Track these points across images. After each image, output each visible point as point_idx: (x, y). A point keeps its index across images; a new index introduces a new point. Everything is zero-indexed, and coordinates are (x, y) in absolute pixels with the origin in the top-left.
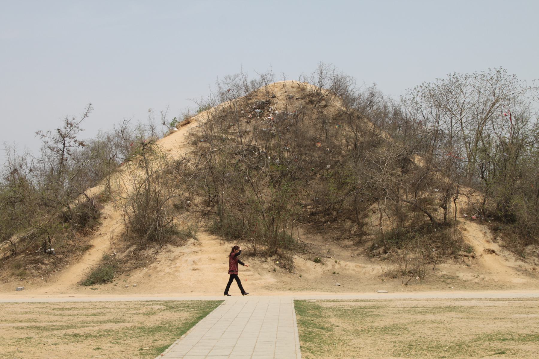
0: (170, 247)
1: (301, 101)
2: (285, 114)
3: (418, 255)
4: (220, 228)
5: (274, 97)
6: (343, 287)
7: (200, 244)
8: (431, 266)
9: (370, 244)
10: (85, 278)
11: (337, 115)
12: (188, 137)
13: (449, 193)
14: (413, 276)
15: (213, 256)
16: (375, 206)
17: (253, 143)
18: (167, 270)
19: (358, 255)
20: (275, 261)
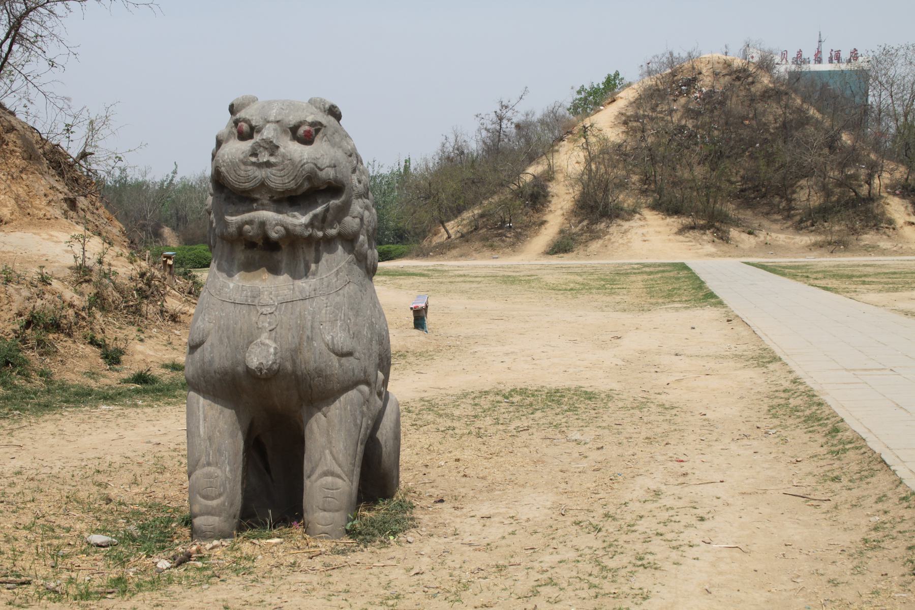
0: (620, 222)
1: (727, 78)
2: (712, 92)
3: (843, 227)
4: (660, 205)
5: (700, 73)
6: (775, 254)
7: (645, 219)
8: (855, 237)
9: (798, 218)
10: (548, 250)
11: (765, 92)
12: (617, 117)
13: (874, 169)
14: (838, 245)
15: (658, 229)
16: (803, 182)
17: (683, 122)
18: (621, 241)
19: (787, 228)
20: (713, 233)
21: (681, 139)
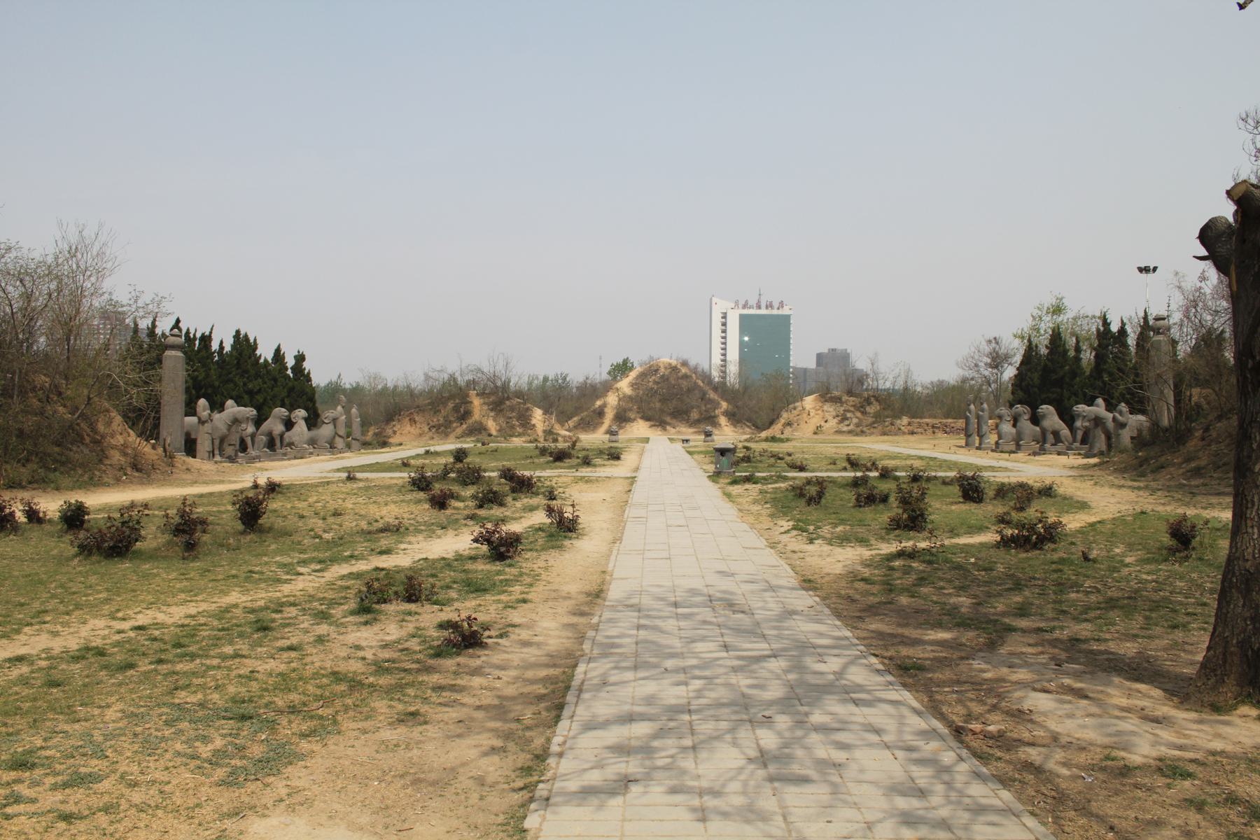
21: (652, 393)
